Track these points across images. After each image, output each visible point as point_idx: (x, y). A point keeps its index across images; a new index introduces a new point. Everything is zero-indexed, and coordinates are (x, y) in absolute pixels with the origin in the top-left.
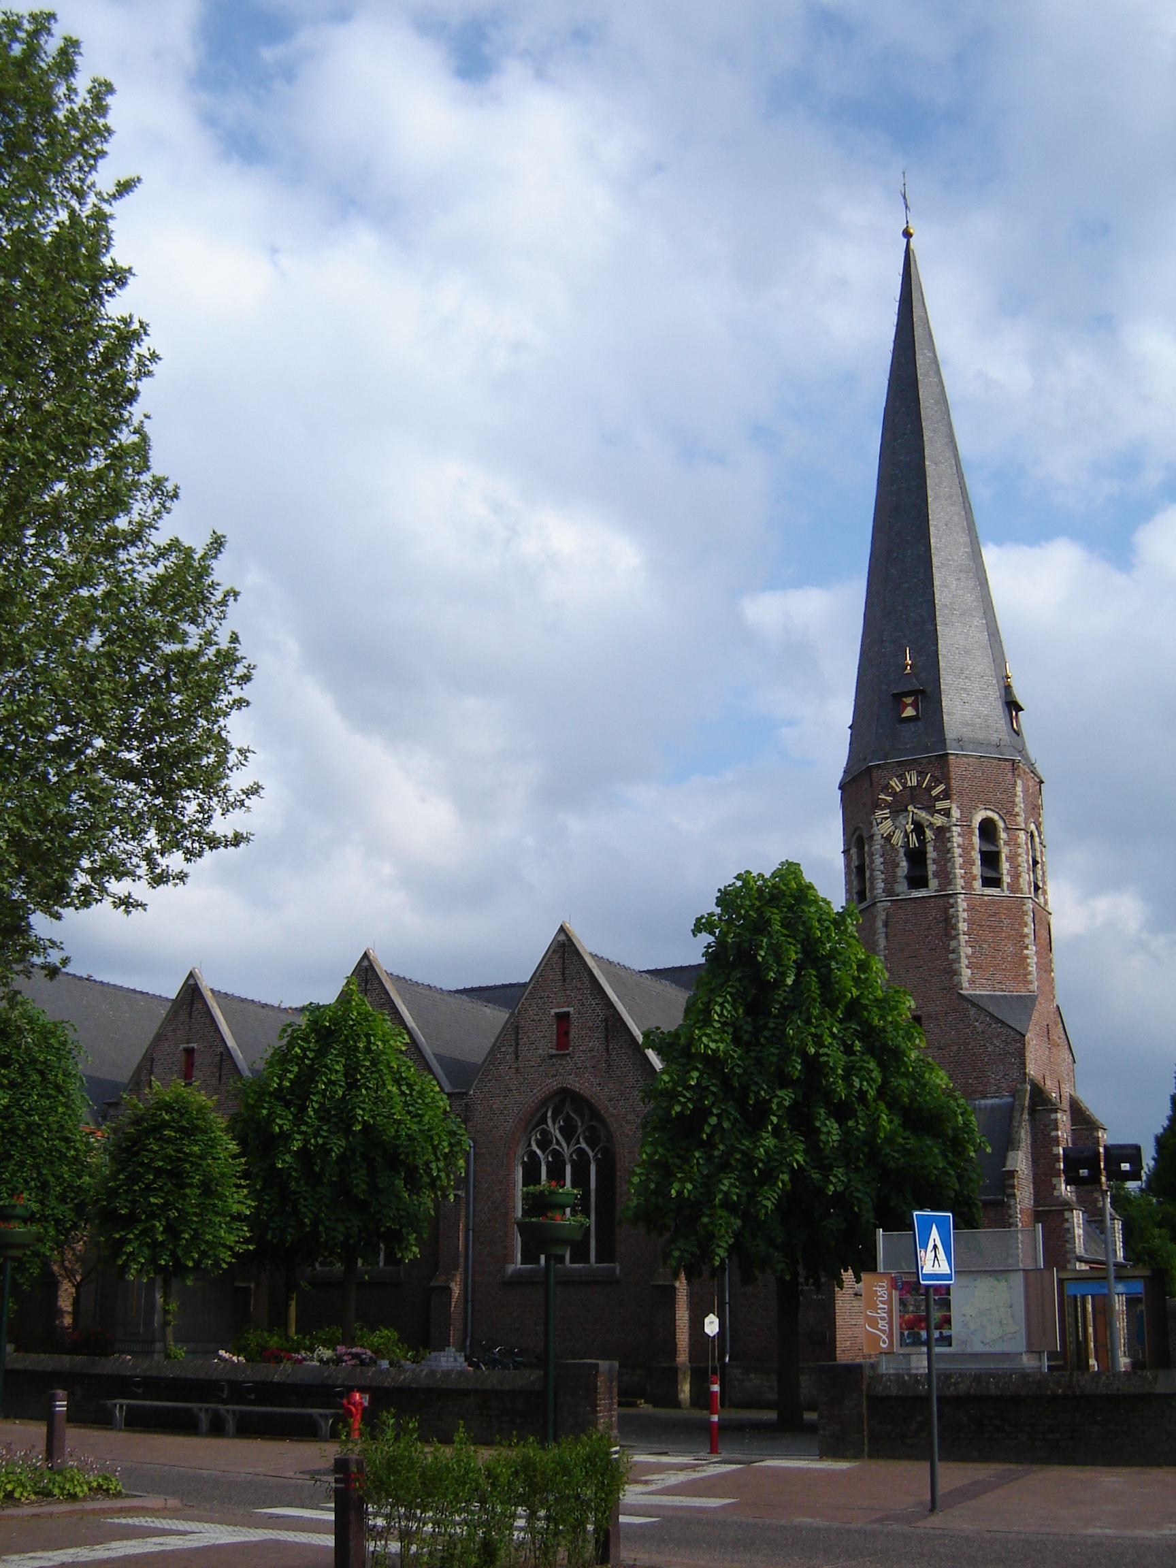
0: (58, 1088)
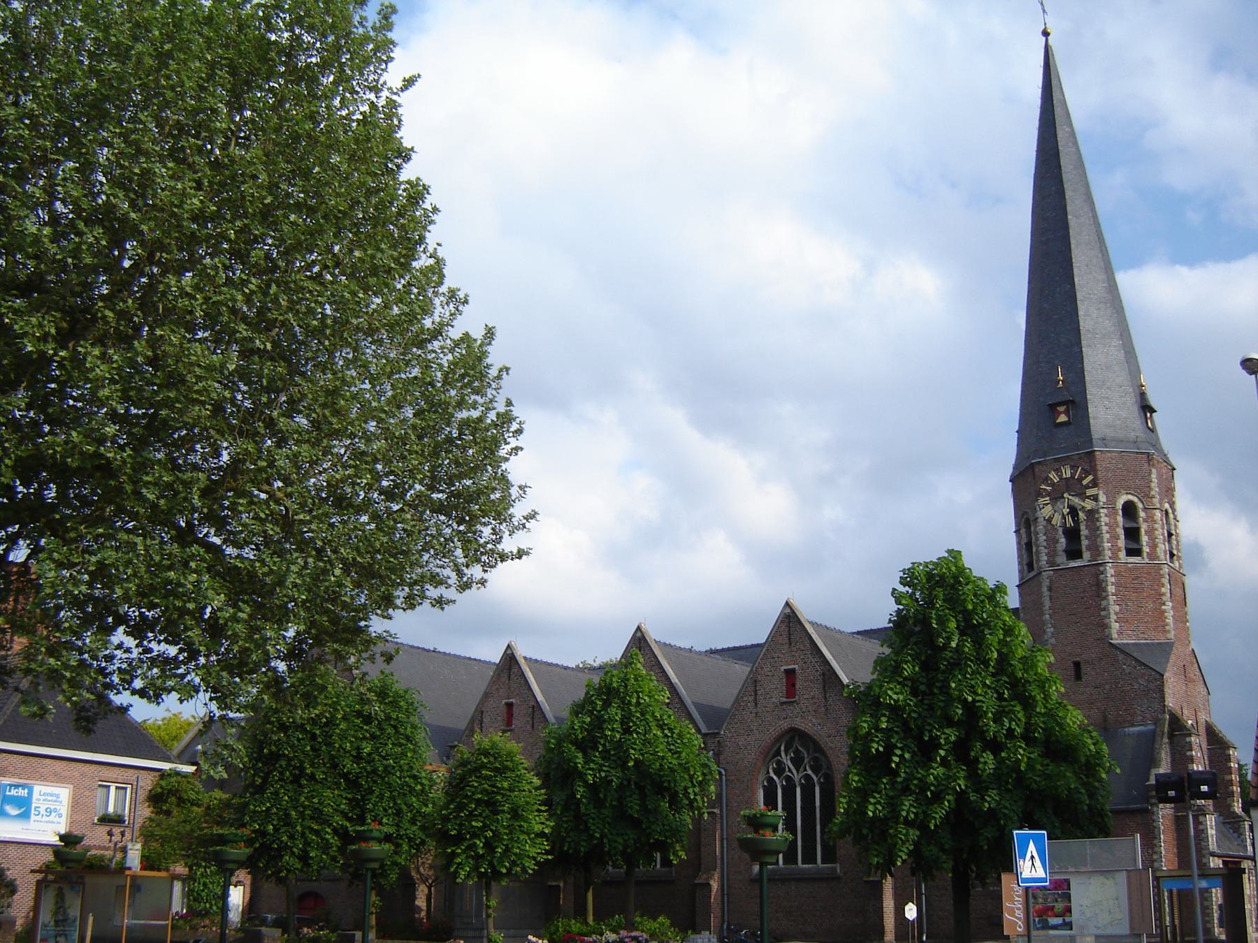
0: (408, 738)
